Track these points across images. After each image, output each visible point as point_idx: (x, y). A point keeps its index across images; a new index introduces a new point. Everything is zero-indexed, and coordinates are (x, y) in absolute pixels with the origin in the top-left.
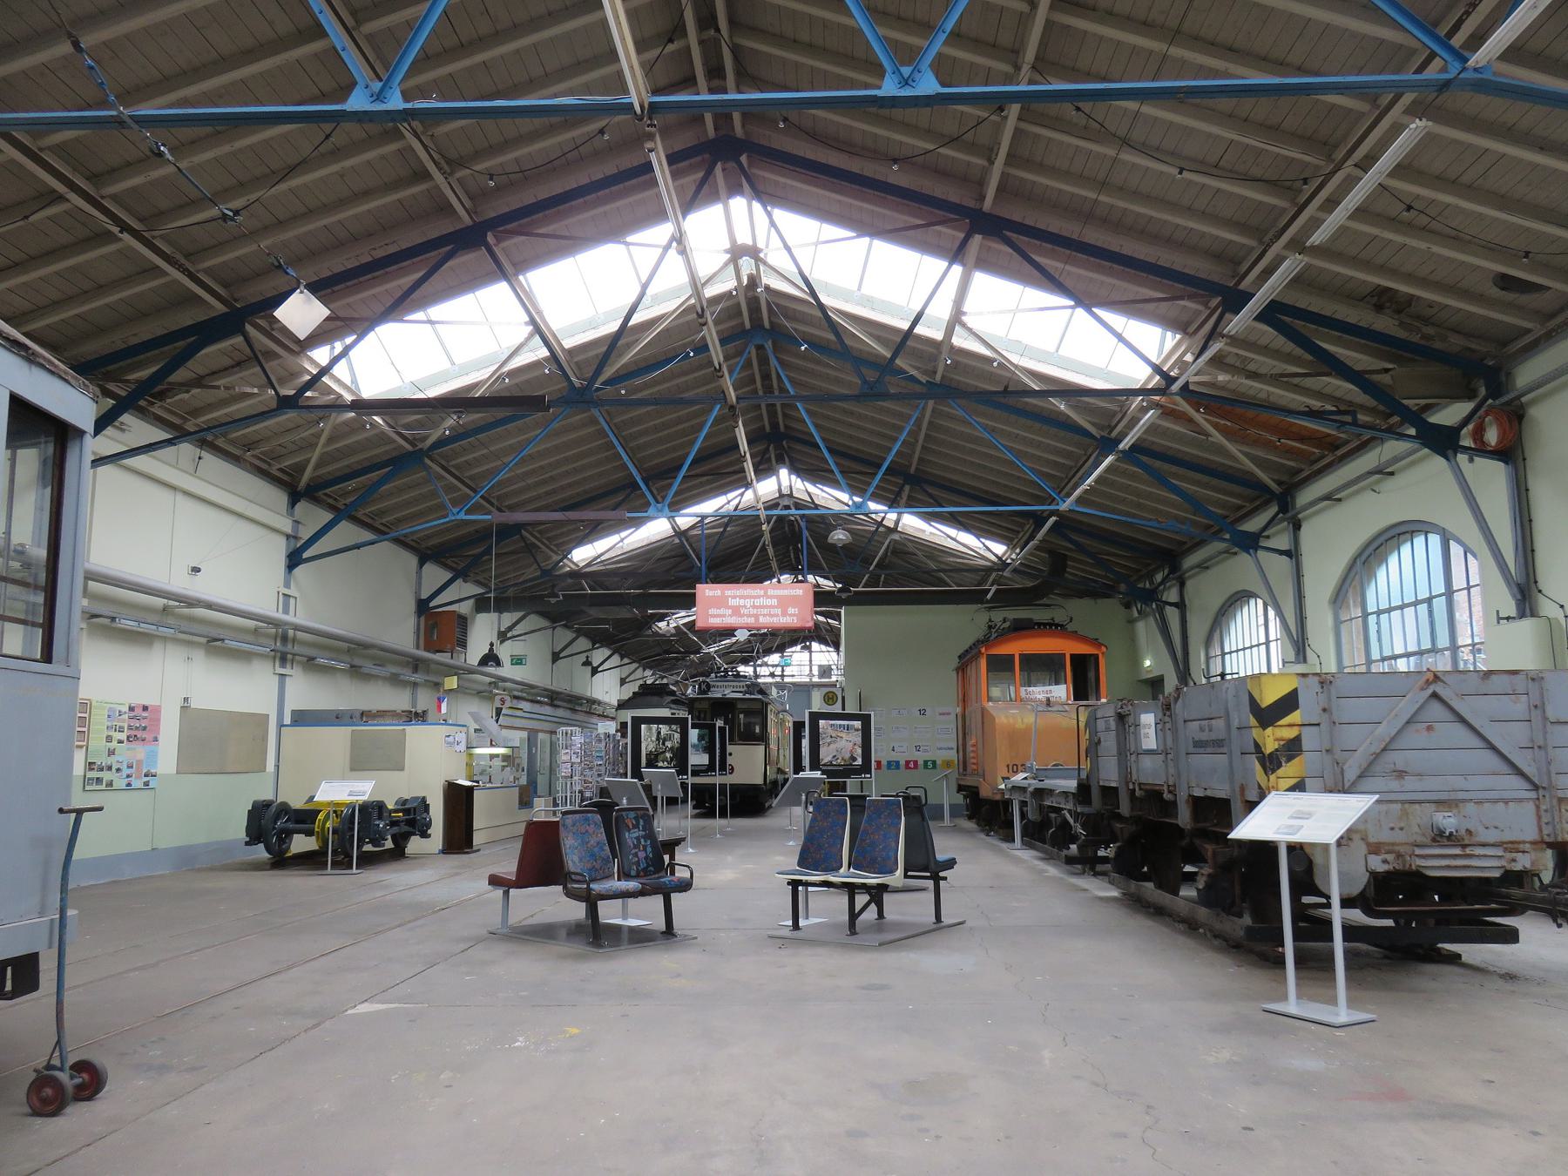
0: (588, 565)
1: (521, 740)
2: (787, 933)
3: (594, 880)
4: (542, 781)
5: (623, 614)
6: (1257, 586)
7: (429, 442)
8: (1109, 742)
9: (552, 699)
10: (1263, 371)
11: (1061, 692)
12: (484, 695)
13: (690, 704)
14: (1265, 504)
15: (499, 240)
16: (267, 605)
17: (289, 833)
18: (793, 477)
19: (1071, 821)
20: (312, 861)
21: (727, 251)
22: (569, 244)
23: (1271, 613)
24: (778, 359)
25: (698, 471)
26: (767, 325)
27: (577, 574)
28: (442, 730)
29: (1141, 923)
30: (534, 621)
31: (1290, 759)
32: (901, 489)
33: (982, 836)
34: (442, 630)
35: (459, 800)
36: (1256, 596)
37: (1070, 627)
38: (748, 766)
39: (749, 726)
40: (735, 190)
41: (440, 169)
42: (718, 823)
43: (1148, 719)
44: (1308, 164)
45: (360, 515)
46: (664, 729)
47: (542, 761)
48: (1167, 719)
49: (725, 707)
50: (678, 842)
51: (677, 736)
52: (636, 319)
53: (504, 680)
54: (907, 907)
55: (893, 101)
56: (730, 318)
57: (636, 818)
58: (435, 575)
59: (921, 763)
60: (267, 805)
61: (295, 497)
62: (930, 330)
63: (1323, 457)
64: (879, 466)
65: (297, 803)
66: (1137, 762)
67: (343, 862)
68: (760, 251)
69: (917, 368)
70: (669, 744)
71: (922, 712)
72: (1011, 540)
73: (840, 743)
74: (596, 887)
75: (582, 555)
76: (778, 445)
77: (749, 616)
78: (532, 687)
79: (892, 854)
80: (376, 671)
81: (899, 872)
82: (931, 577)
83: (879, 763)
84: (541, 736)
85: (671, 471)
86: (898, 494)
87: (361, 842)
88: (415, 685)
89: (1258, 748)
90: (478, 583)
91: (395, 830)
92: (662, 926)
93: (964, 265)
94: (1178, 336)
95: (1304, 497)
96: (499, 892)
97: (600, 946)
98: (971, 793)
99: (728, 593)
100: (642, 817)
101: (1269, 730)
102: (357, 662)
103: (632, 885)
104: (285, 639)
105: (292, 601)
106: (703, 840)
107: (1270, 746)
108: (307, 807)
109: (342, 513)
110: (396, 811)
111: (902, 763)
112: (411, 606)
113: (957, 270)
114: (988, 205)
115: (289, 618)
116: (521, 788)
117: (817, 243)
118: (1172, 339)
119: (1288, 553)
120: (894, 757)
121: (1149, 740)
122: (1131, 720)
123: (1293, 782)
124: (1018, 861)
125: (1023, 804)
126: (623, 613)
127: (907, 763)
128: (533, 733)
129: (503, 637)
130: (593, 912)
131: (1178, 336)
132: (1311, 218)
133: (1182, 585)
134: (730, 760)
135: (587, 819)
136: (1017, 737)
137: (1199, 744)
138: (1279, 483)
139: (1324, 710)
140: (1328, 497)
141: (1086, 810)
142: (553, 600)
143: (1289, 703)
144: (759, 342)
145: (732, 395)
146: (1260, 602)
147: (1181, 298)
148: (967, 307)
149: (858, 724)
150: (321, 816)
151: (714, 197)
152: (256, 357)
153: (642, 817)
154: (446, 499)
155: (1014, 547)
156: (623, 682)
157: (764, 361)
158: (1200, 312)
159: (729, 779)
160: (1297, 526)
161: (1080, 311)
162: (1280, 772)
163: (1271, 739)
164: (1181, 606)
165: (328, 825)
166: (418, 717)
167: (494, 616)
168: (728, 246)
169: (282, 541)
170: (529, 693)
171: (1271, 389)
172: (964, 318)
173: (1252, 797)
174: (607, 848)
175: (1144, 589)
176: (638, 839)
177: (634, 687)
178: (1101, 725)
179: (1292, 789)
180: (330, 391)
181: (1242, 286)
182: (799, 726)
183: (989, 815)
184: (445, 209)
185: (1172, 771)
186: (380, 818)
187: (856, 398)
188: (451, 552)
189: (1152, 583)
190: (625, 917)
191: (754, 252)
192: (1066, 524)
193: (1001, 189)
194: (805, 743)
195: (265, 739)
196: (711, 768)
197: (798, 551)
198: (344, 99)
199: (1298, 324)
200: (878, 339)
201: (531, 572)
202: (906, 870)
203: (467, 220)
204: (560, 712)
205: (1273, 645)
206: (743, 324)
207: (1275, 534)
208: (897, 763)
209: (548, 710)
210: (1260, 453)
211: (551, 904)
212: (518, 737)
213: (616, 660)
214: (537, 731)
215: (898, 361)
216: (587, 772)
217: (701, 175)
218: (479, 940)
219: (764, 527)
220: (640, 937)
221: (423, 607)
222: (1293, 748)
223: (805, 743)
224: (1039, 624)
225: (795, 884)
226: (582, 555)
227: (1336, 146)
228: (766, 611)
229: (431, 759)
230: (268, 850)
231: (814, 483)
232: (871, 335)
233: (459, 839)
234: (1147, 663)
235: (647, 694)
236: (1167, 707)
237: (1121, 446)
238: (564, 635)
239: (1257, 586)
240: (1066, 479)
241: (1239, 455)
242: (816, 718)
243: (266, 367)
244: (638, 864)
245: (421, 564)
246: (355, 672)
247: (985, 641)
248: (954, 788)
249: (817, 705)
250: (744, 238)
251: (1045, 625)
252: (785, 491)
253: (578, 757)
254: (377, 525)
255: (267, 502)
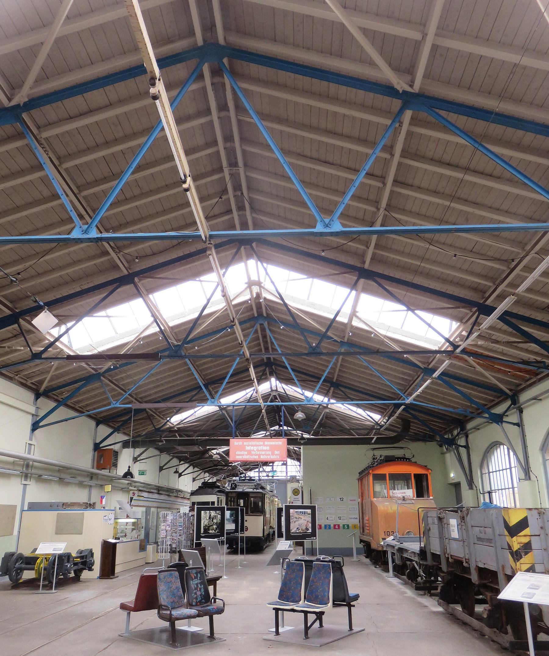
0: (178, 424)
1: (142, 512)
2: (272, 636)
3: (174, 608)
4: (152, 538)
5: (196, 447)
6: (503, 440)
7: (103, 370)
8: (435, 530)
9: (159, 490)
10: (499, 339)
11: (410, 493)
12: (124, 490)
13: (227, 494)
14: (505, 400)
15: (140, 280)
16: (20, 451)
17: (22, 570)
18: (278, 382)
19: (417, 568)
20: (32, 584)
21: (246, 283)
22: (175, 281)
23: (512, 454)
24: (270, 330)
25: (233, 380)
26: (265, 315)
27: (171, 430)
28: (101, 513)
29: (456, 630)
30: (152, 451)
31: (526, 554)
32: (330, 389)
33: (373, 567)
34: (105, 457)
35: (109, 550)
36: (503, 444)
37: (413, 460)
38: (255, 526)
39: (256, 504)
40: (249, 257)
41: (114, 251)
42: (240, 557)
43: (453, 522)
44: (513, 252)
45: (69, 403)
46: (213, 513)
47: (153, 522)
48: (463, 524)
49: (244, 495)
50: (218, 579)
51: (219, 516)
52: (206, 312)
53: (136, 482)
54: (335, 617)
55: (322, 234)
56: (248, 311)
57: (197, 573)
58: (104, 430)
59: (341, 526)
60: (12, 555)
61: (38, 396)
62: (343, 319)
63: (530, 379)
64: (320, 379)
65: (27, 553)
66: (449, 543)
67: (48, 587)
68: (262, 283)
69: (336, 335)
70: (215, 521)
71: (342, 499)
72: (383, 413)
73: (300, 522)
74: (175, 613)
75: (176, 419)
76: (269, 368)
77: (255, 455)
78: (150, 485)
79: (326, 594)
80: (73, 480)
81: (330, 604)
82: (343, 431)
83: (320, 527)
84: (152, 509)
85: (219, 380)
86: (328, 391)
87: (58, 574)
88: (91, 486)
89: (510, 547)
90: (125, 434)
91: (76, 567)
92: (208, 633)
93: (357, 291)
94: (458, 324)
95: (524, 397)
96: (125, 613)
97: (176, 647)
98: (367, 545)
99: (245, 443)
100: (199, 572)
101: (515, 538)
102: (62, 476)
103: (193, 611)
104: (28, 466)
105: (33, 447)
106: (231, 569)
107: (516, 547)
108: (32, 555)
109: (60, 403)
110: (77, 558)
111: (332, 526)
112: (91, 446)
113: (354, 292)
114: (366, 266)
115: (30, 456)
116: (141, 541)
117: (288, 280)
118: (455, 325)
119: (517, 425)
120: (328, 522)
121: (455, 534)
122: (445, 521)
123: (528, 566)
124: (391, 585)
125: (393, 554)
126: (196, 448)
127: (335, 526)
128: (148, 508)
129: (135, 460)
130: (173, 625)
131: (458, 324)
132: (518, 275)
133: (467, 437)
134: (246, 524)
135: (171, 575)
136: (389, 517)
137: (479, 539)
138: (511, 390)
139: (542, 528)
140: (535, 398)
141: (425, 563)
142: (160, 444)
143: (523, 524)
144: (262, 322)
145: (248, 354)
146: (505, 447)
147: (459, 308)
148: (358, 309)
149: (309, 511)
150: (38, 561)
151: (240, 259)
152: (22, 333)
153: (199, 572)
154: (109, 395)
155: (384, 417)
156: (194, 480)
157: (263, 330)
158: (467, 314)
159: (247, 534)
160: (521, 411)
161: (410, 312)
162: (522, 561)
163: (516, 543)
164: (467, 447)
165: (41, 566)
166: (90, 506)
167: (131, 450)
168: (247, 281)
169: (30, 417)
170: (147, 488)
171: (504, 348)
172: (357, 314)
173: (509, 573)
174: (181, 590)
175: (448, 439)
176: (197, 584)
177: (199, 483)
178: (430, 520)
179: (528, 570)
180: (58, 347)
181: (489, 302)
182: (280, 510)
183: (377, 557)
184: (115, 267)
185: (467, 552)
186: (68, 562)
187: (306, 354)
188: (113, 420)
189: (452, 435)
190: (189, 626)
191: (259, 284)
192: (409, 407)
193: (372, 259)
194: (283, 519)
195: (14, 518)
196: (236, 531)
197: (280, 417)
198: (69, 233)
199: (514, 321)
200: (318, 322)
201: (150, 428)
202: (334, 601)
203: (126, 272)
204: (162, 497)
205: (513, 469)
206: (253, 314)
207: (510, 415)
208: (330, 526)
209: (156, 496)
210: (500, 376)
211: (150, 619)
212: (140, 512)
213: (191, 469)
214: (150, 507)
215: (328, 333)
216: (174, 535)
217: (235, 250)
218: (113, 641)
219: (263, 411)
220: (196, 640)
221: (97, 447)
222: (527, 547)
223: (283, 519)
224: (398, 458)
225: (277, 610)
226: (176, 419)
227: (526, 244)
228: (263, 453)
229: (94, 531)
230: (11, 580)
231: (287, 384)
232: (314, 320)
233: (108, 571)
234: (452, 475)
235: (206, 488)
236: (463, 518)
237: (434, 376)
238: (165, 457)
239: (503, 440)
240: (408, 388)
241: (490, 377)
242: (288, 508)
243: (27, 337)
244: (196, 598)
245: (97, 425)
246: (62, 481)
247: (371, 467)
248: (359, 541)
249: (290, 498)
250: (254, 278)
251: (401, 458)
252: (274, 388)
253: (172, 524)
254: (77, 407)
255: (23, 399)
